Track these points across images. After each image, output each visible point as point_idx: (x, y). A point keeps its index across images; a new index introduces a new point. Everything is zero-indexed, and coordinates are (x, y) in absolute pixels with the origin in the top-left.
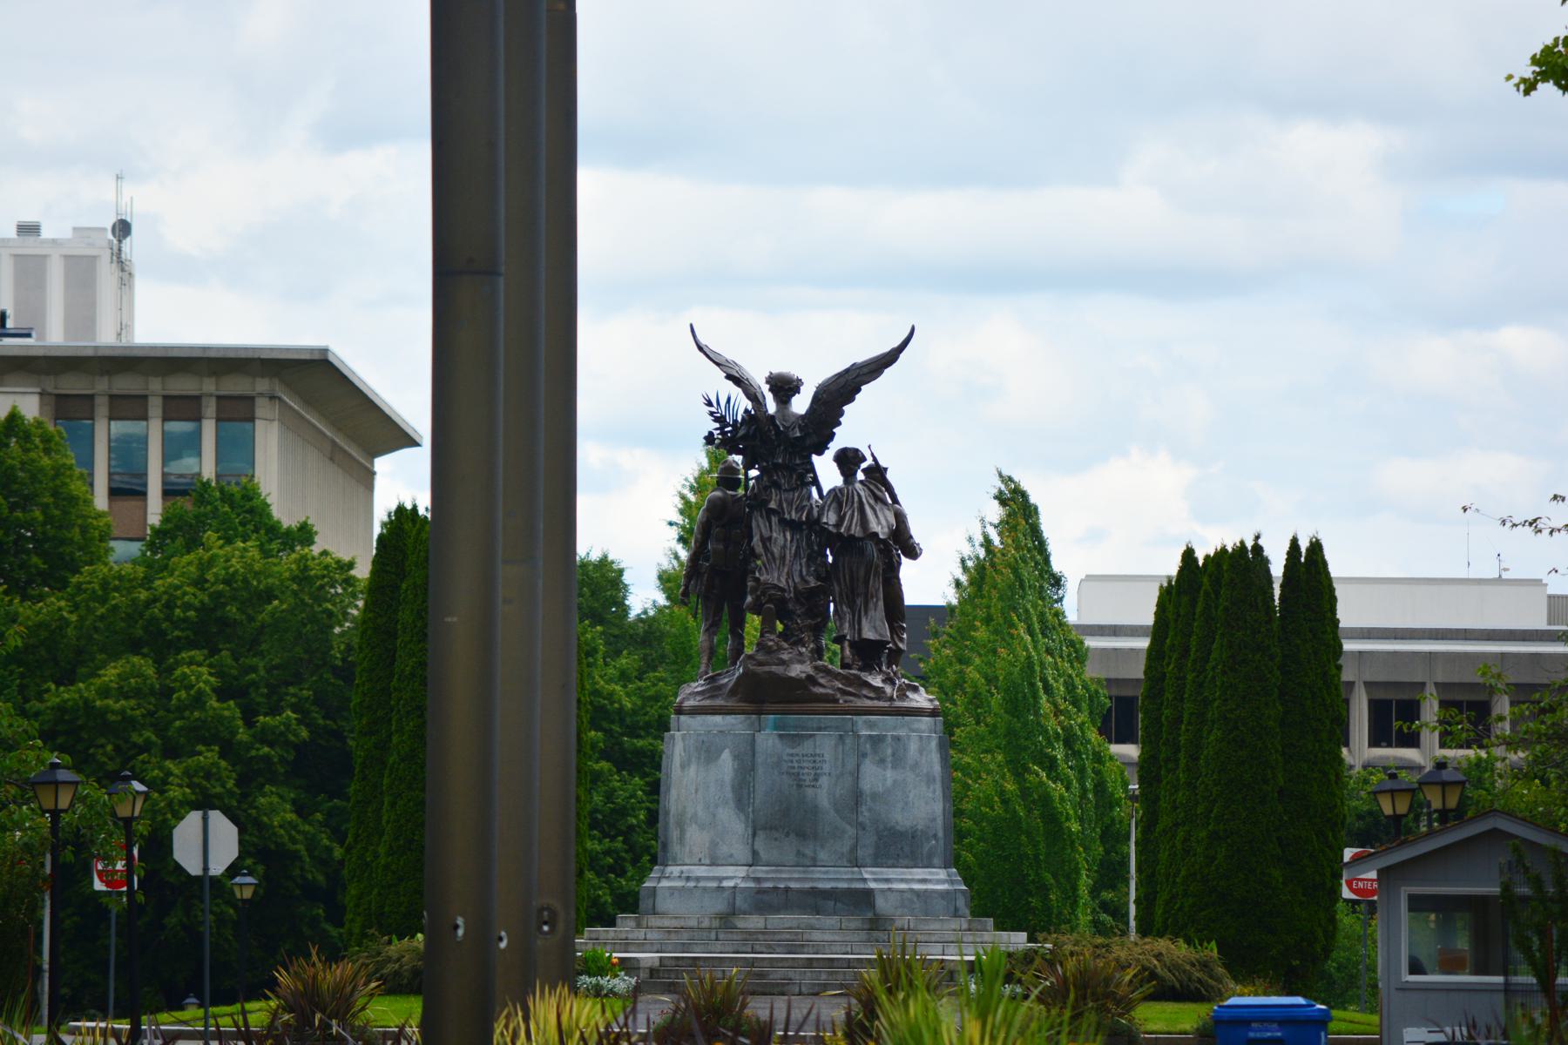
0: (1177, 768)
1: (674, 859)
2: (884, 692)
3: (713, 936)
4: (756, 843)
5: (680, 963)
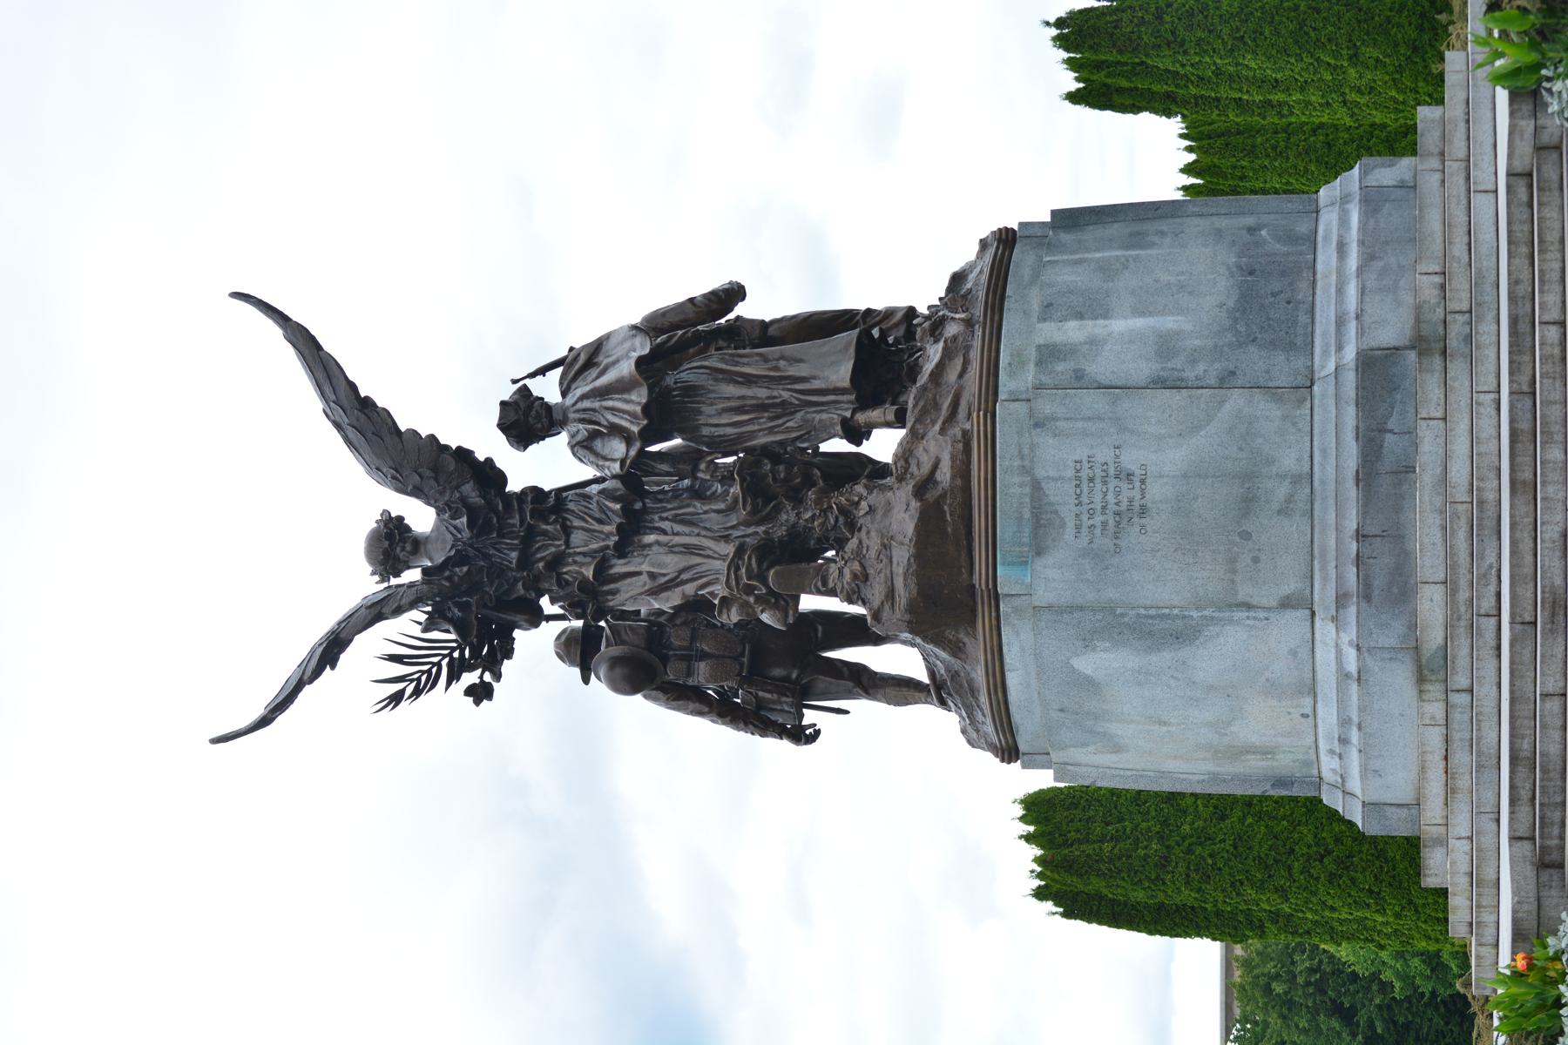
0: (1286, 103)
1: (1307, 764)
2: (955, 338)
3: (1463, 699)
4: (1264, 602)
5: (1525, 794)
